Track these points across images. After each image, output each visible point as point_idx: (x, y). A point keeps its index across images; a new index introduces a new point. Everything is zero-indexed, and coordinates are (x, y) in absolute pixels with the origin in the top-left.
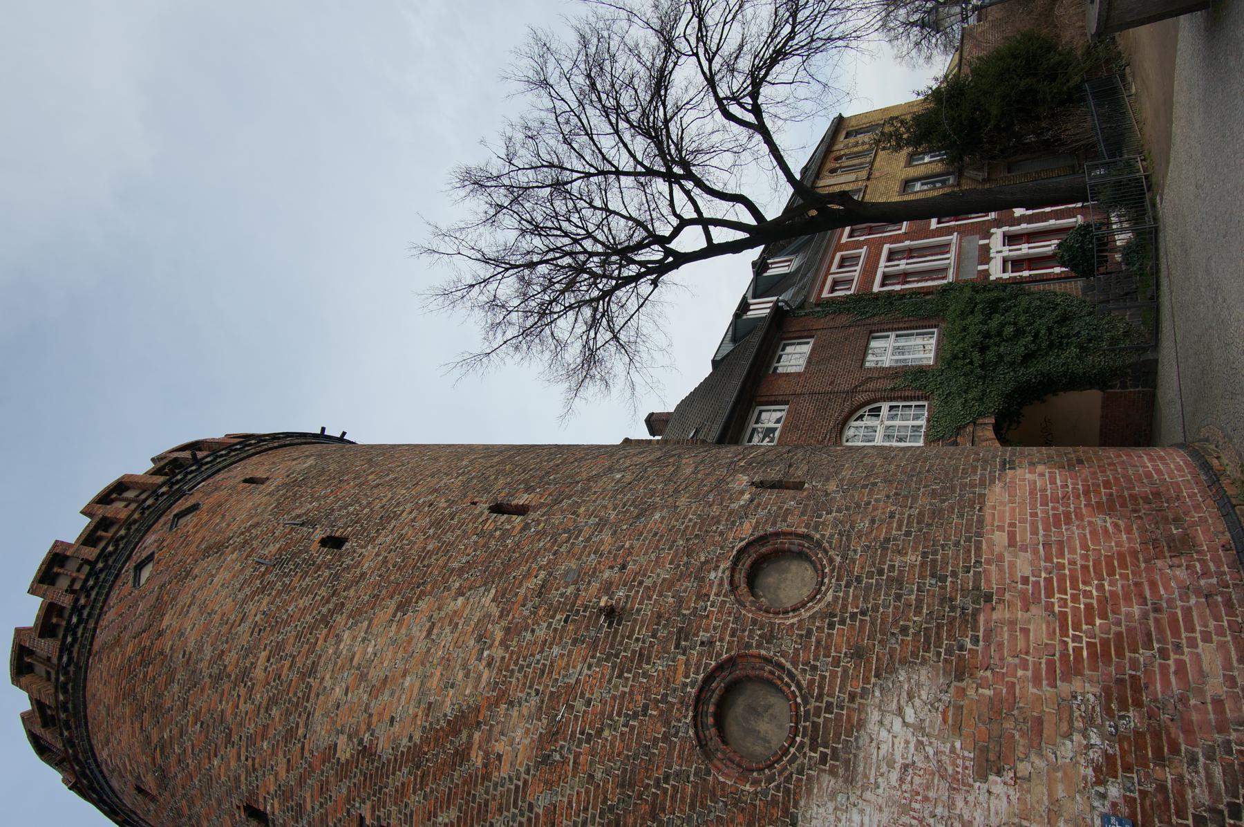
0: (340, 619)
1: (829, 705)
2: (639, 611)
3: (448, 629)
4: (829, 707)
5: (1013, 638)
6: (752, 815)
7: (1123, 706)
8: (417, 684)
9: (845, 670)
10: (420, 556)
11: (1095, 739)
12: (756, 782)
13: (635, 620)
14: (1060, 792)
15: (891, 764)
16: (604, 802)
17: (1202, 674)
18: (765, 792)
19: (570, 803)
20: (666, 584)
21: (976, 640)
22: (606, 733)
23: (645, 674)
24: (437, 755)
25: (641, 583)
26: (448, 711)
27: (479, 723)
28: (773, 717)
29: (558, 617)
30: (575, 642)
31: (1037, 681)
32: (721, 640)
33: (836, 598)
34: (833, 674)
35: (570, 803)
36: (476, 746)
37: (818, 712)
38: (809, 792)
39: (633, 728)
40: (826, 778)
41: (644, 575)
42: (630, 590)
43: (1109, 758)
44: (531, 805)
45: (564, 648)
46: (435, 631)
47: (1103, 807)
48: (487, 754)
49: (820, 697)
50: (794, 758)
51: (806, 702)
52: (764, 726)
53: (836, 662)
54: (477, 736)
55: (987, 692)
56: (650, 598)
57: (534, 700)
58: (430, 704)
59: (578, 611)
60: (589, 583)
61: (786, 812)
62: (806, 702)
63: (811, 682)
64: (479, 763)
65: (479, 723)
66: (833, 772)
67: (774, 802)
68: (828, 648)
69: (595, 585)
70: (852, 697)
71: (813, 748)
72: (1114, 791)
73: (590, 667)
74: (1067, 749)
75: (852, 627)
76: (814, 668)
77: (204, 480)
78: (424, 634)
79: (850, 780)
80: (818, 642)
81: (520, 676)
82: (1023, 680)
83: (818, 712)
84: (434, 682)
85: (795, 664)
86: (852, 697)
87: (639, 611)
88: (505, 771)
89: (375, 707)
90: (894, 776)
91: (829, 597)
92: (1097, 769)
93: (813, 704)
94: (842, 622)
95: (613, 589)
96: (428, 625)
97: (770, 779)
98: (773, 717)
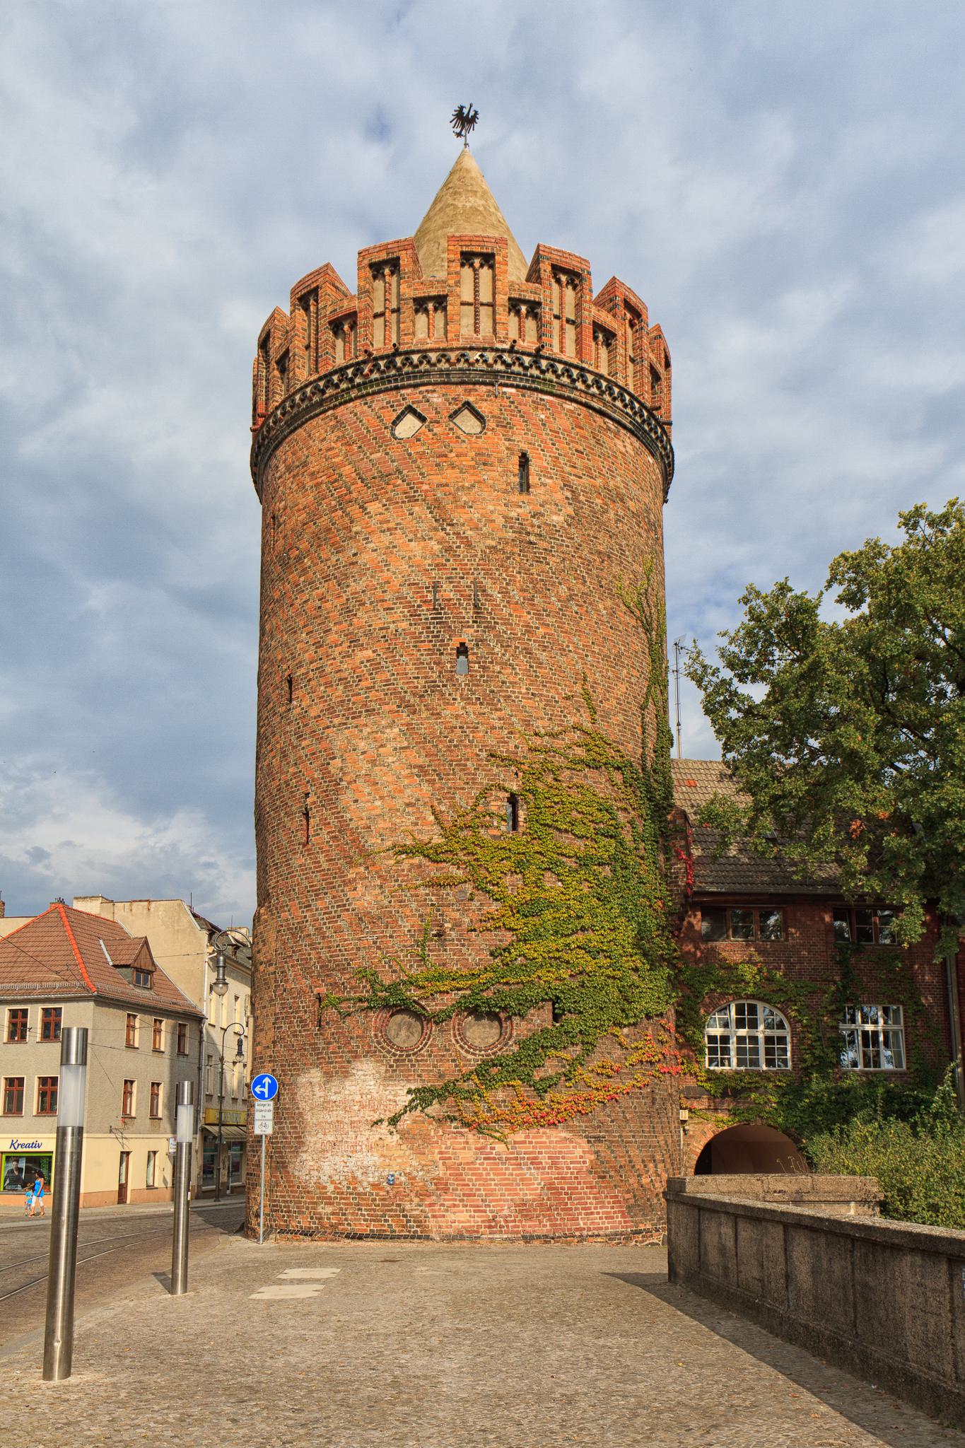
0: (405, 717)
1: (414, 1066)
2: (445, 950)
3: (413, 818)
4: (414, 1066)
5: (460, 1143)
6: (363, 1037)
7: (436, 1184)
8: (378, 811)
9: (431, 1071)
10: (461, 760)
11: (421, 1173)
12: (376, 1036)
13: (439, 950)
14: (399, 1160)
15: (395, 1095)
16: (352, 960)
17: (454, 1213)
18: (372, 1041)
19: (346, 940)
20: (465, 962)
21: (455, 1128)
22: (379, 952)
23: (411, 966)
24: (347, 844)
25: (463, 945)
26: (369, 843)
27: (367, 868)
28: (408, 1037)
29: (433, 898)
30: (421, 916)
31: (441, 1153)
32: (436, 1005)
33: (470, 1060)
34: (428, 1066)
35: (346, 940)
36: (357, 870)
37: (410, 1061)
38: (377, 1061)
39: (384, 967)
40: (383, 1068)
41: (469, 945)
42: (458, 940)
43: (414, 1178)
44: (339, 916)
45: (416, 910)
46: (410, 809)
47: (396, 1175)
48: (355, 880)
49: (418, 1061)
50: (389, 1052)
51: (414, 1054)
52: (403, 1033)
53: (435, 1066)
54: (362, 869)
55: (432, 1134)
56: (454, 955)
57: (386, 902)
58: (369, 827)
59: (438, 910)
60: (458, 910)
61: (368, 1052)
62: (414, 1054)
63: (423, 1056)
64: (350, 876)
65: (367, 868)
66: (387, 1071)
67: (370, 1046)
68: (441, 1060)
69: (457, 915)
70: (419, 1076)
71: (394, 1061)
72: (403, 1179)
73: (409, 931)
74: (415, 1163)
75: (455, 1071)
76: (430, 1056)
77: (517, 387)
78: (407, 801)
79: (385, 1079)
80: (443, 1056)
81: (396, 887)
82: (440, 1148)
83: (410, 1061)
84: (382, 825)
85: (431, 1045)
86: (419, 1076)
87: (445, 950)
88: (350, 895)
89: (360, 782)
90: (390, 1097)
91: (469, 1057)
92: (409, 1174)
93: (413, 1058)
94: (456, 1066)
95: (457, 929)
96: (413, 801)
97: (379, 1043)
98: (408, 1037)
